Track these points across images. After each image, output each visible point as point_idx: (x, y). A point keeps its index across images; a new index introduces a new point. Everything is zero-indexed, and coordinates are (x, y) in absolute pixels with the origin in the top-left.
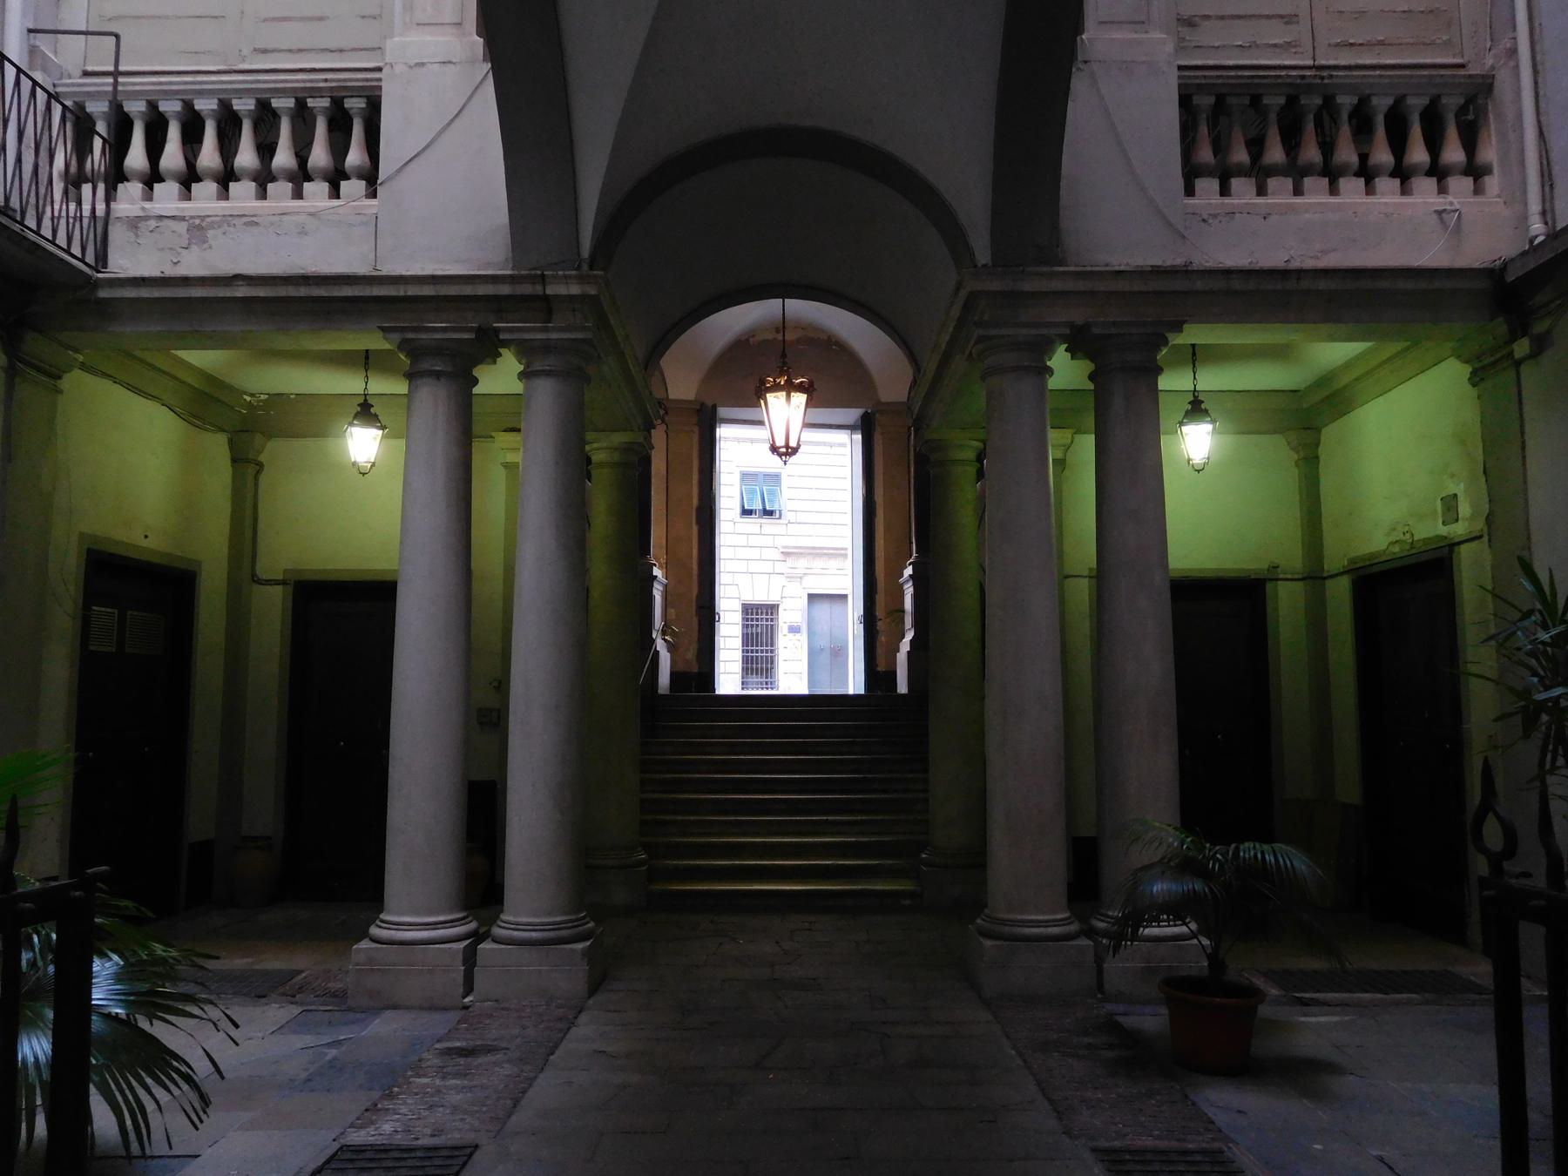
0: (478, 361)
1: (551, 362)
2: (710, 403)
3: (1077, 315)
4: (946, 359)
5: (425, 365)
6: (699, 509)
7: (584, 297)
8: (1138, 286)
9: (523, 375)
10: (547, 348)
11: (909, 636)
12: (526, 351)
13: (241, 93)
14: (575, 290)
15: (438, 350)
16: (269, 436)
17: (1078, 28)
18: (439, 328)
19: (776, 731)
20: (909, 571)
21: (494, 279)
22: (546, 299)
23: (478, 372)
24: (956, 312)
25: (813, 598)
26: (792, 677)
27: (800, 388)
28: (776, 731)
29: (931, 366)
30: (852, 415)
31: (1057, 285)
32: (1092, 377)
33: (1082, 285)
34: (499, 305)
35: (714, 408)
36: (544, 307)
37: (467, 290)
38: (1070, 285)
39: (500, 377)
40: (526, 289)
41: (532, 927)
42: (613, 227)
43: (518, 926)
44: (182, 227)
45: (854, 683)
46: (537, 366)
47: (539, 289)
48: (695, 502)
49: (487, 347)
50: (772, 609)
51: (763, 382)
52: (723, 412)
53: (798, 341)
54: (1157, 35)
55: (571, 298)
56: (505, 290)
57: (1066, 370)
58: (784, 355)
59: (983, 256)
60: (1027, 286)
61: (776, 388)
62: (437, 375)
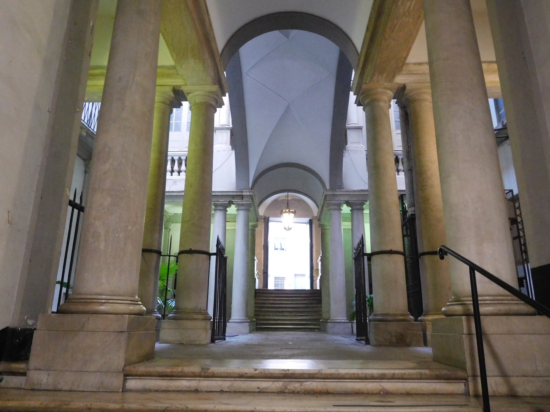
0: (227, 207)
1: (243, 208)
2: (267, 217)
3: (346, 199)
4: (323, 206)
5: (219, 208)
6: (264, 245)
7: (250, 195)
8: (358, 193)
9: (238, 210)
10: (242, 205)
11: (320, 275)
12: (238, 205)
13: (183, 156)
14: (248, 194)
15: (221, 205)
16: (173, 222)
17: (346, 144)
18: (222, 201)
19: (287, 297)
20: (320, 258)
21: (232, 192)
22: (242, 195)
23: (227, 209)
24: (323, 198)
25: (295, 275)
26: (289, 285)
27: (292, 212)
28: (287, 297)
29: (320, 207)
30: (307, 220)
31: (342, 193)
32: (351, 211)
33: (347, 193)
34: (233, 197)
35: (269, 218)
36: (242, 197)
37: (227, 194)
38: (345, 193)
39: (232, 210)
40: (239, 194)
41: (239, 319)
42: (255, 181)
43: (235, 319)
44: (172, 181)
45: (307, 287)
46: (240, 208)
47: (241, 194)
48: (263, 243)
49: (230, 203)
50: (283, 278)
51: (282, 211)
52: (271, 219)
53: (292, 200)
54: (362, 145)
55: (247, 195)
56: (235, 194)
57: (346, 209)
58: (288, 204)
59: (328, 187)
60: (336, 193)
61: (286, 212)
62: (221, 210)
